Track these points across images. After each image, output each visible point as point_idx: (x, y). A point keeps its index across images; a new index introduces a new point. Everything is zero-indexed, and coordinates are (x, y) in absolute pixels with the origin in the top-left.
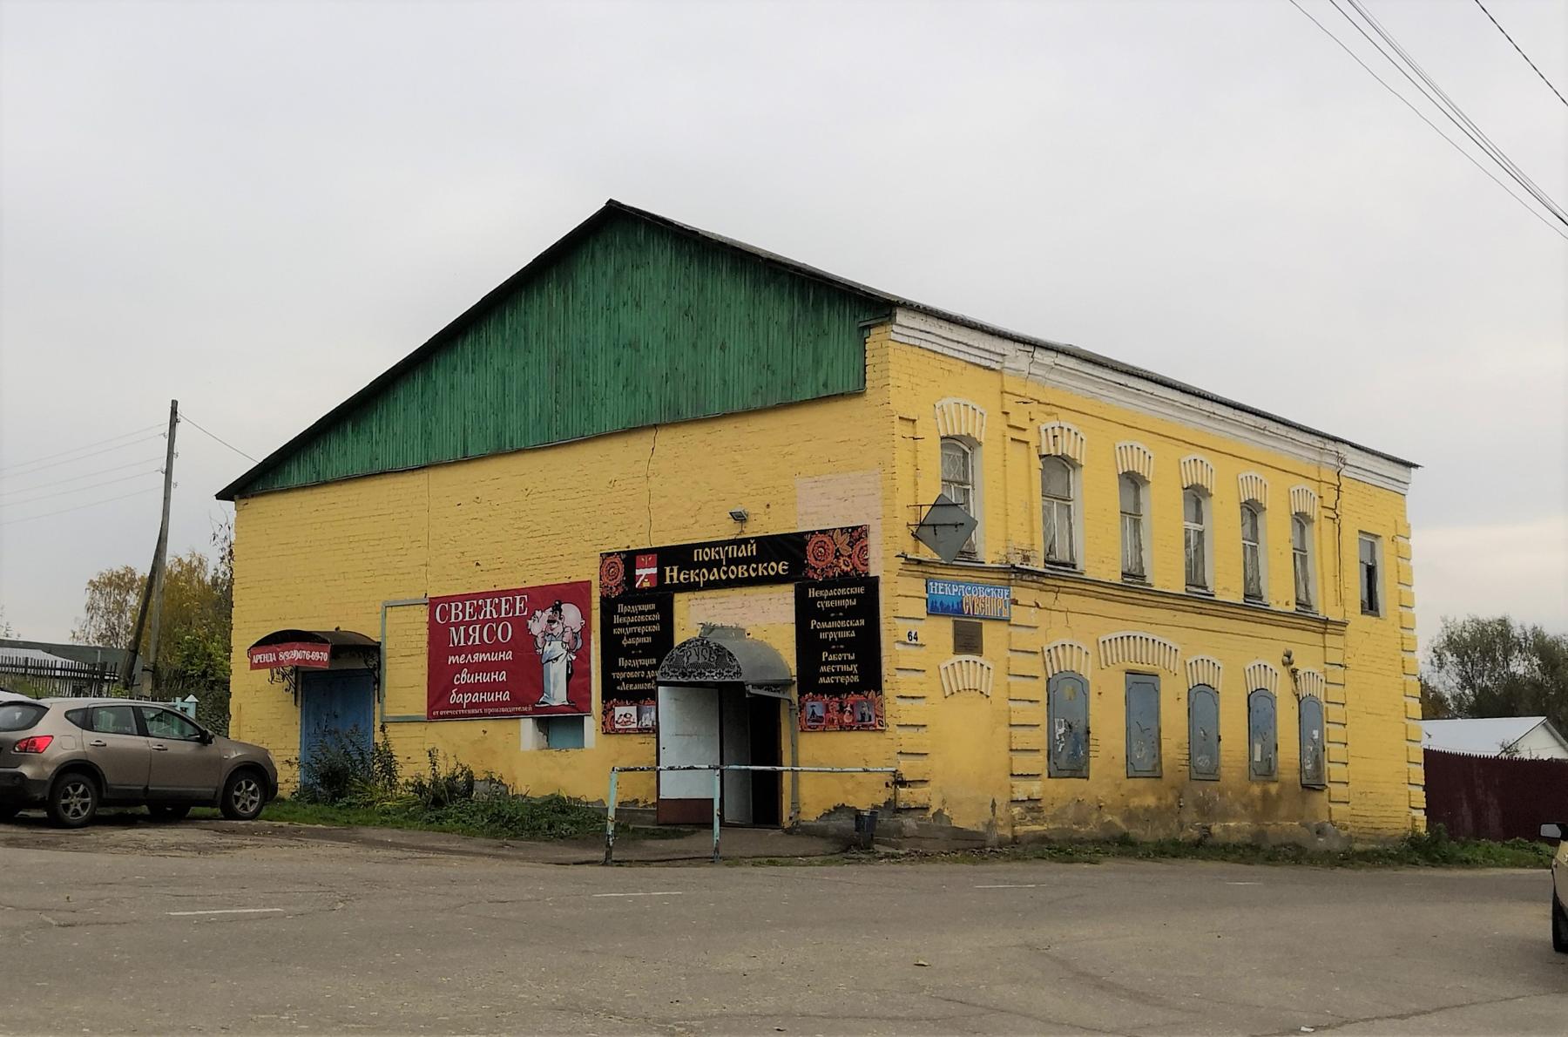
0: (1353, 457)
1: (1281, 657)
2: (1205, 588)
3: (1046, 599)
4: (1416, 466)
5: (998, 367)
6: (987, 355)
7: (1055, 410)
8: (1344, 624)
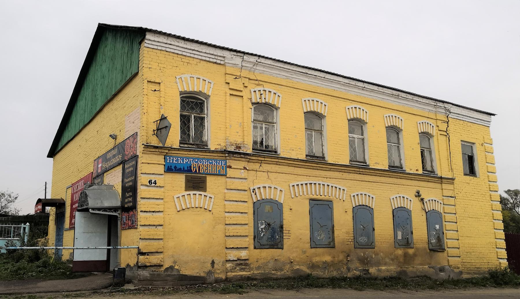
0: (454, 109)
1: (414, 193)
2: (366, 163)
3: (256, 166)
4: (494, 115)
5: (222, 63)
6: (213, 57)
7: (261, 83)
8: (453, 179)
